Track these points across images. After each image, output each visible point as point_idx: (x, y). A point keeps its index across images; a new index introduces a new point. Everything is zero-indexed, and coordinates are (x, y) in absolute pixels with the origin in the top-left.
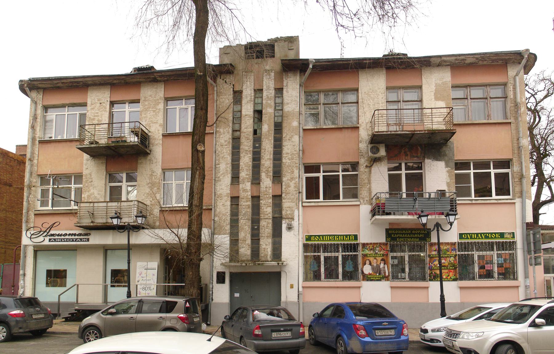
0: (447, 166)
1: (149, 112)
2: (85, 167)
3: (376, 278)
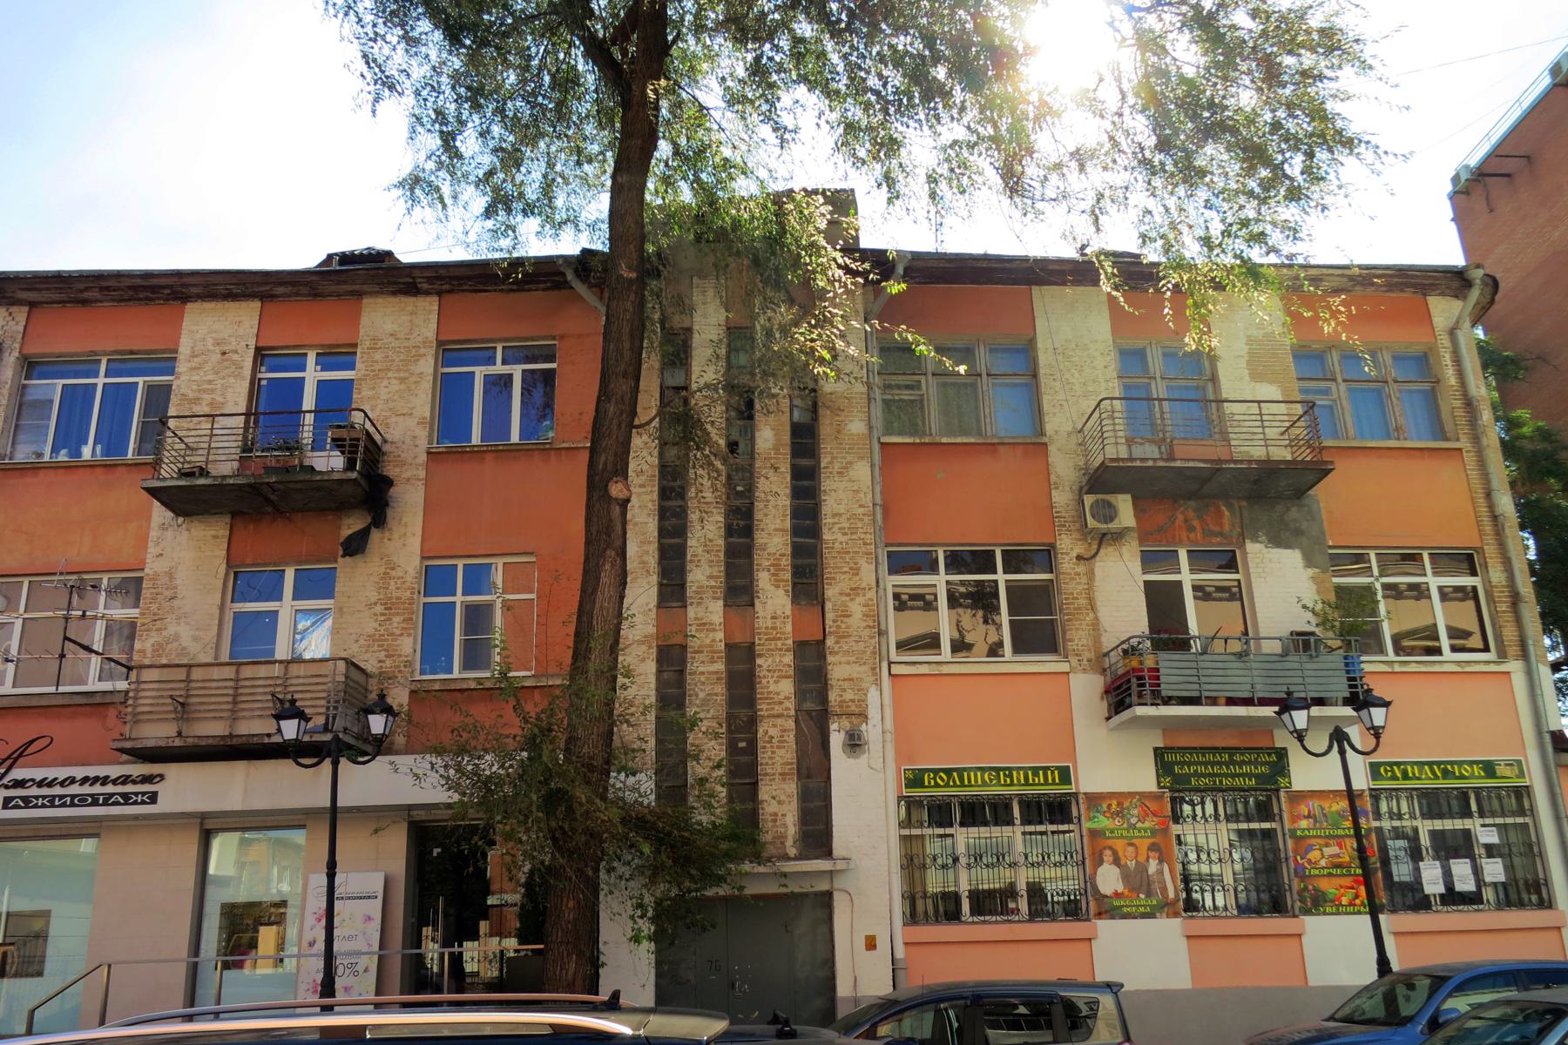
0: (1309, 562)
1: (385, 383)
2: (152, 550)
3: (1137, 906)
